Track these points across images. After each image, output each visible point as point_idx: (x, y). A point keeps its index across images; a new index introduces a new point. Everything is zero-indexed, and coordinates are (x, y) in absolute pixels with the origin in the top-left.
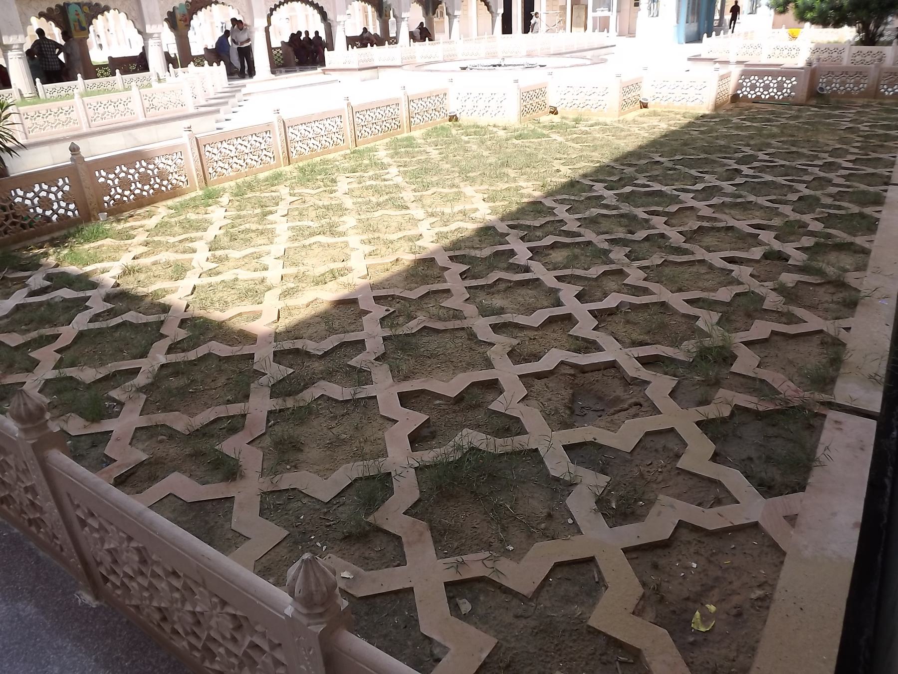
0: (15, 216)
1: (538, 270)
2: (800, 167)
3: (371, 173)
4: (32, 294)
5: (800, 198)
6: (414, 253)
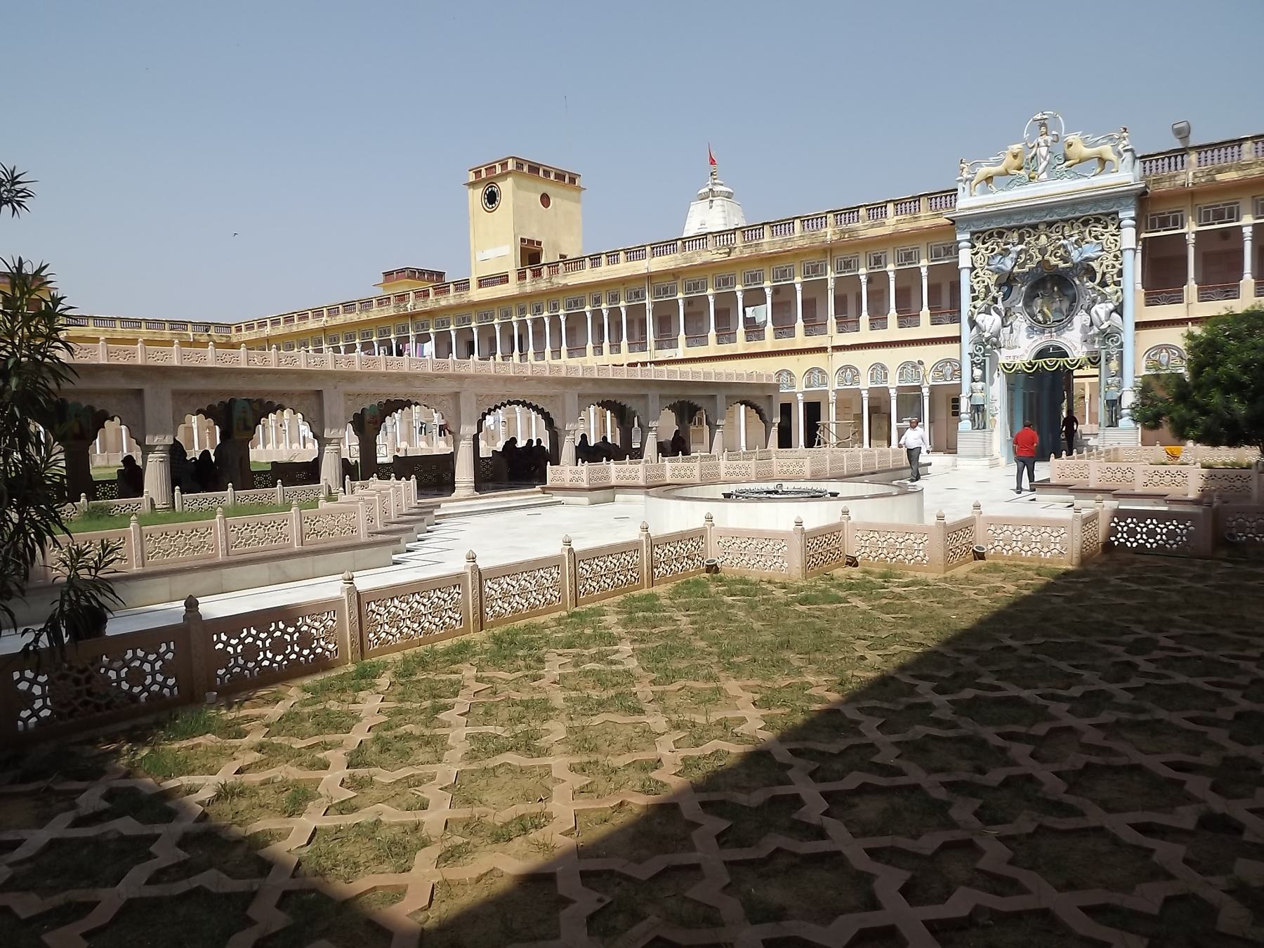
0: (90, 693)
1: (840, 838)
2: (1226, 660)
3: (593, 651)
4: (79, 822)
5: (1238, 716)
6: (647, 793)
